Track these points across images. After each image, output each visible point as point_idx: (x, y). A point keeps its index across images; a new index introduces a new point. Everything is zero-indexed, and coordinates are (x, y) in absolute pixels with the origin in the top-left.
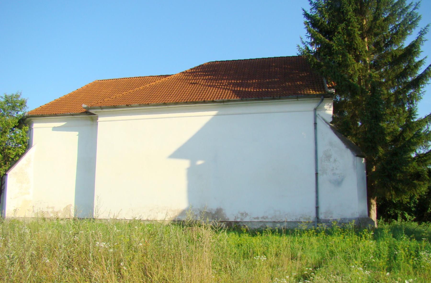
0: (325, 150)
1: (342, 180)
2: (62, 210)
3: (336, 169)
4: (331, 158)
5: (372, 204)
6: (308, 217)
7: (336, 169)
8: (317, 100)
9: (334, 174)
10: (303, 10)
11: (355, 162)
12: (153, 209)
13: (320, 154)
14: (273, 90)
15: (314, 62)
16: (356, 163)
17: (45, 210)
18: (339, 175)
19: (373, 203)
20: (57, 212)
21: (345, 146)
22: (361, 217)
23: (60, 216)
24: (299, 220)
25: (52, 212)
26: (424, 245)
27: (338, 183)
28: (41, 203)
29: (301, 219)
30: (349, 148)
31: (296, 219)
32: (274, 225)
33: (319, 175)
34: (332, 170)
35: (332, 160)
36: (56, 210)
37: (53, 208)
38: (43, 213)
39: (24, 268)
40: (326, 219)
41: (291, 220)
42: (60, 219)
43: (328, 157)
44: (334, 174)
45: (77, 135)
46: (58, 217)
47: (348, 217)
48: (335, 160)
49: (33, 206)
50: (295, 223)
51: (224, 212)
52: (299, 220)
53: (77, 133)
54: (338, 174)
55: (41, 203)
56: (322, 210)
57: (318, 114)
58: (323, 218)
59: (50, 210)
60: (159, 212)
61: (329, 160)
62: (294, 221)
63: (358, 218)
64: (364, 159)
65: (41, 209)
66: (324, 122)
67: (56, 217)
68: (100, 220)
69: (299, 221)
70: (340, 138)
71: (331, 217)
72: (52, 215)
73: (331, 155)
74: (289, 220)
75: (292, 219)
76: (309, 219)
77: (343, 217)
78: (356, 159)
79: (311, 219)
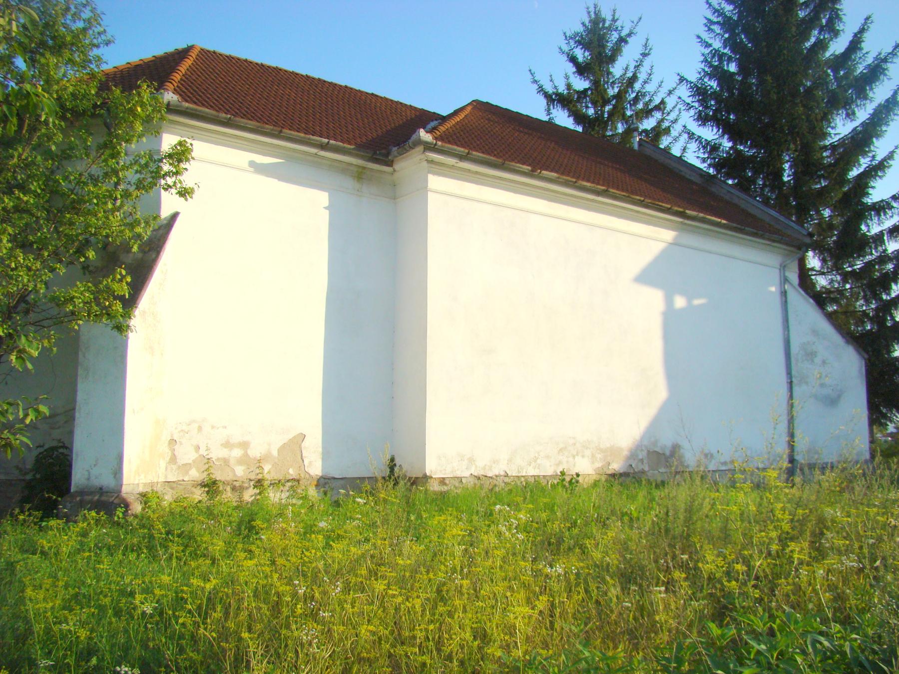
1: (839, 397)
2: (275, 453)
4: (816, 357)
10: (678, 74)
17: (217, 453)
20: (259, 461)
21: (844, 340)
23: (269, 471)
25: (240, 462)
27: (833, 401)
28: (200, 429)
30: (852, 344)
32: (812, 474)
35: (818, 360)
36: (255, 452)
37: (245, 445)
38: (207, 466)
42: (266, 483)
43: (811, 355)
44: (822, 385)
45: (325, 208)
49: (172, 442)
51: (682, 451)
53: (322, 198)
55: (200, 429)
56: (802, 443)
59: (237, 453)
60: (577, 454)
61: (813, 361)
65: (202, 451)
67: (253, 477)
68: (442, 481)
72: (240, 471)
73: (816, 352)
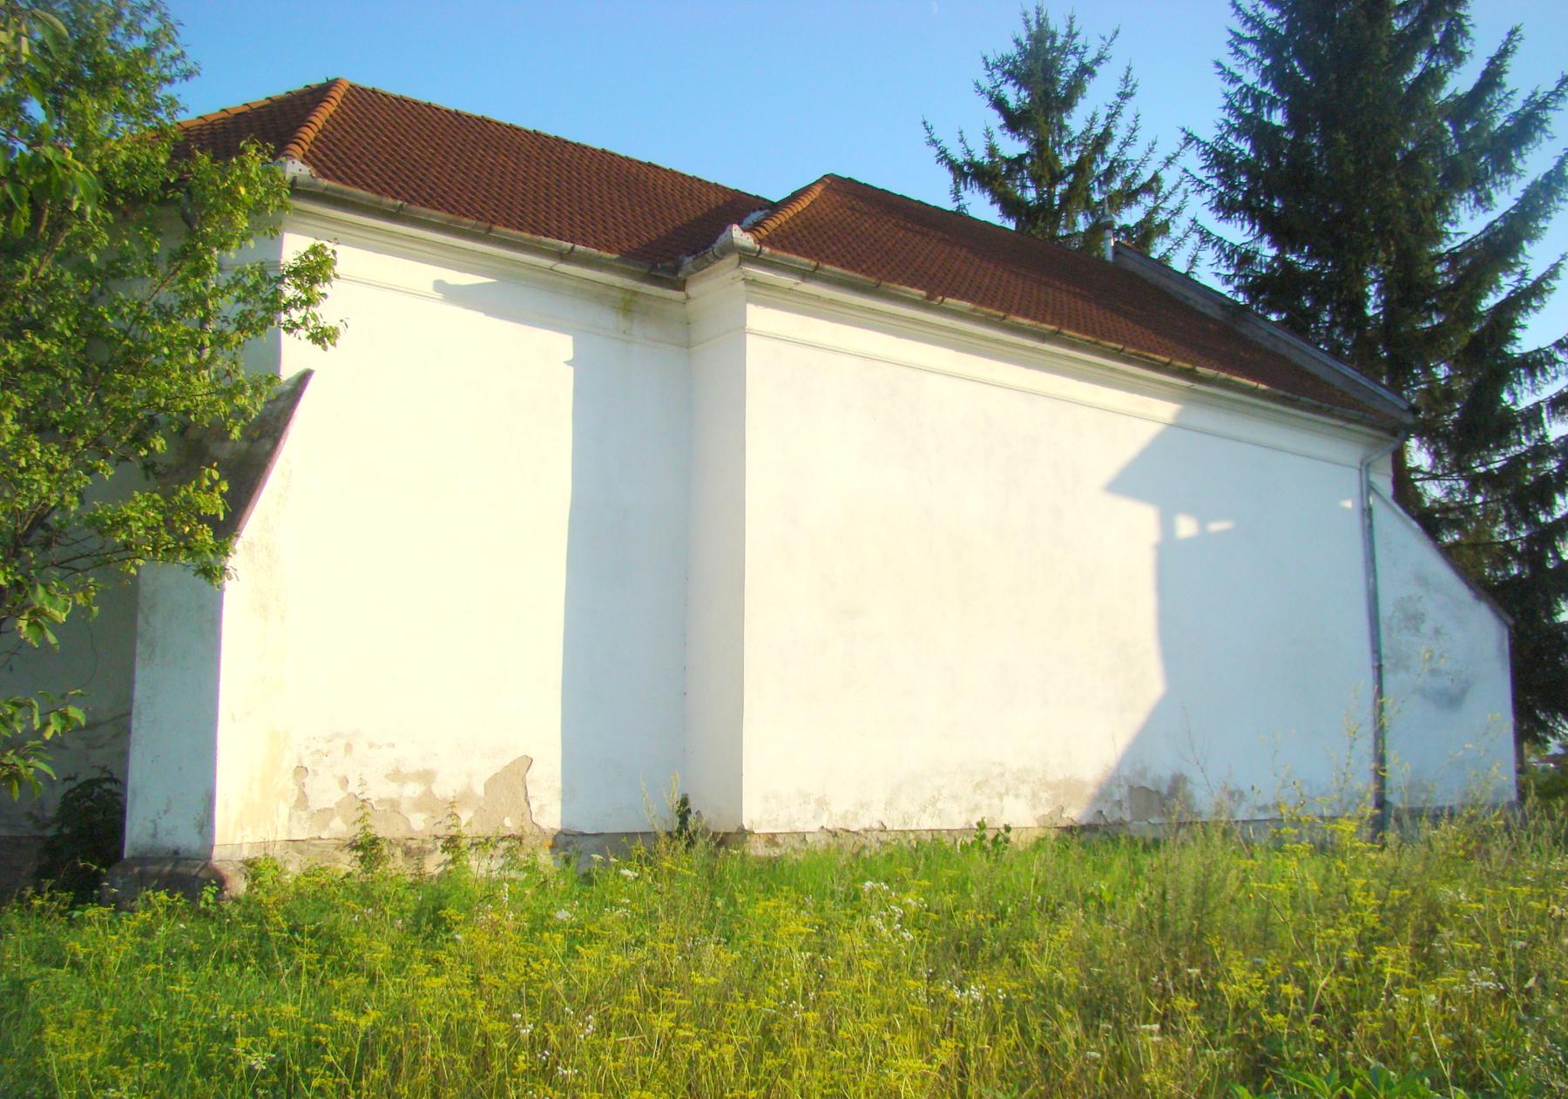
1: (1464, 692)
2: (479, 790)
8: (1369, 435)
9: (1434, 672)
12: (987, 781)
13: (1386, 608)
15: (87, 83)
20: (452, 804)
23: (469, 822)
25: (418, 805)
26: (1357, 833)
27: (1452, 700)
28: (349, 748)
35: (1426, 628)
36: (445, 788)
37: (426, 777)
38: (361, 813)
42: (464, 843)
43: (1414, 620)
44: (1434, 672)
45: (568, 363)
46: (453, 831)
49: (301, 771)
53: (561, 345)
54: (1448, 673)
56: (1398, 772)
59: (413, 790)
61: (1417, 630)
65: (353, 787)
72: (419, 822)
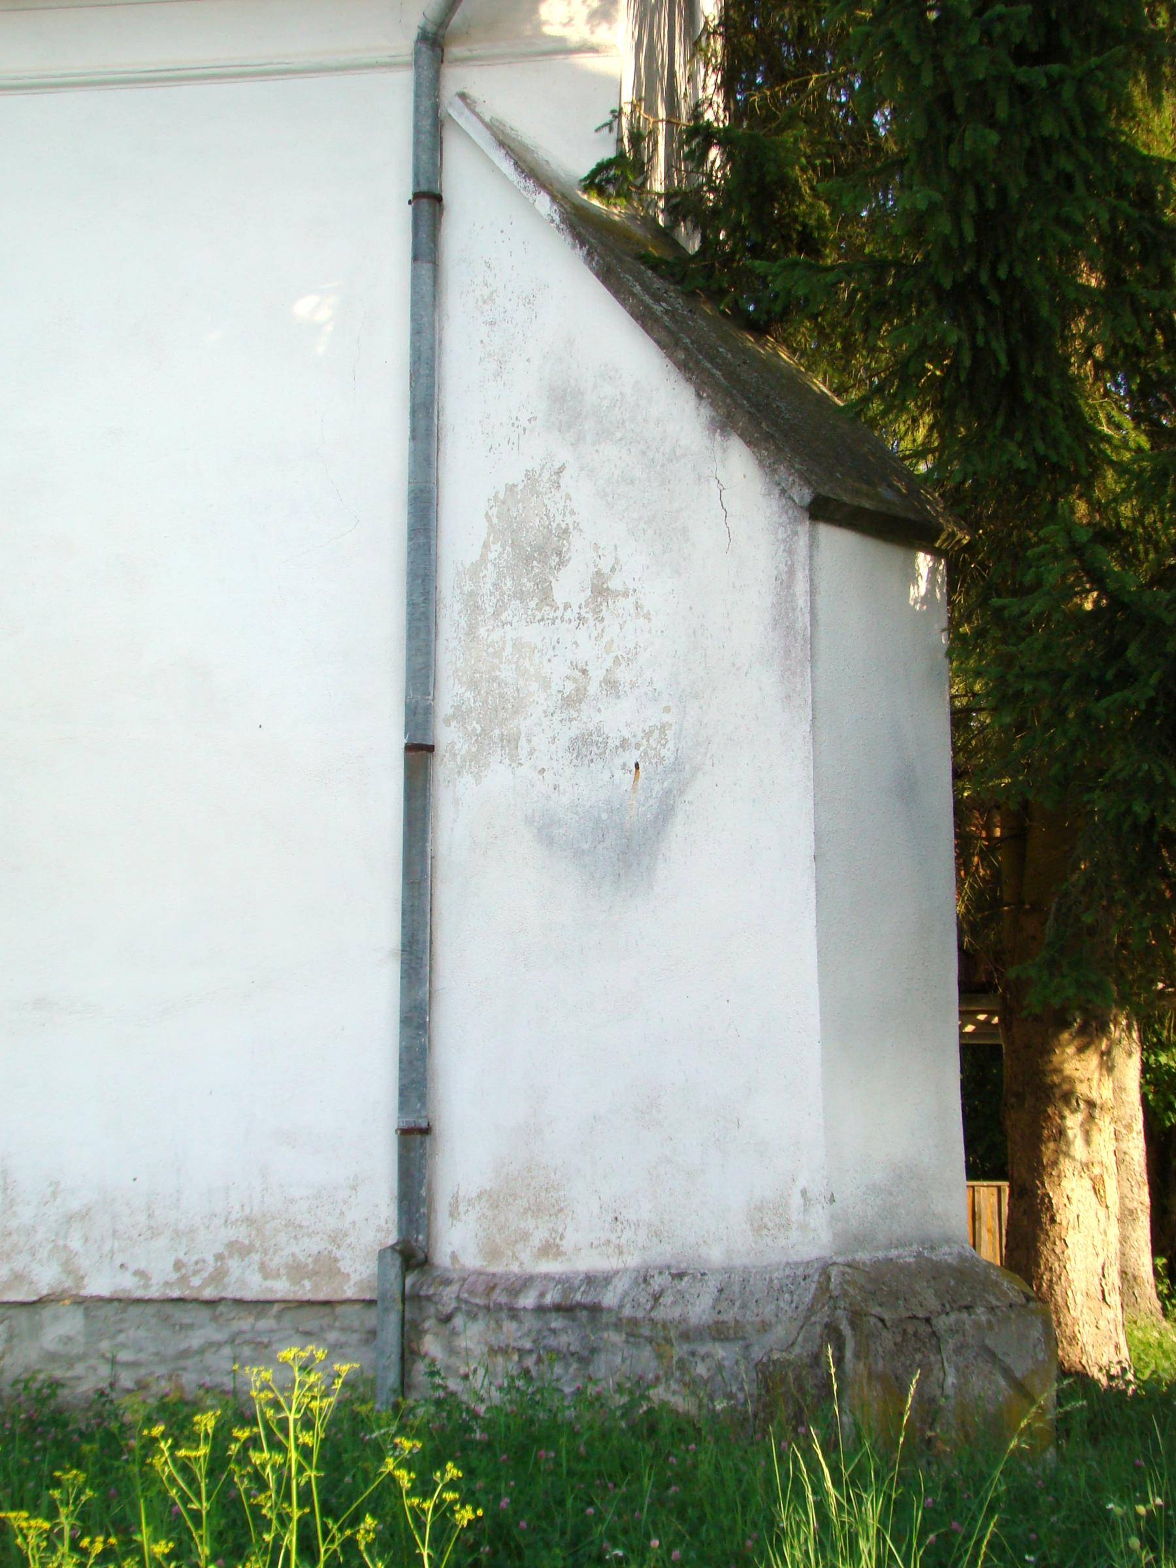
0: (511, 488)
1: (665, 813)
3: (611, 685)
5: (1068, 1097)
6: (314, 1245)
7: (611, 685)
11: (801, 587)
14: (1168, 891)
16: (813, 592)
18: (631, 757)
19: (1081, 1089)
21: (706, 412)
22: (863, 1256)
24: (218, 1276)
29: (234, 1264)
31: (178, 1265)
33: (443, 768)
34: (572, 702)
39: (547, 1241)
40: (497, 1268)
41: (128, 1284)
47: (715, 1255)
48: (600, 591)
50: (169, 1309)
52: (218, 1276)
54: (624, 744)
57: (463, 96)
58: (472, 1260)
61: (546, 596)
62: (154, 1292)
63: (825, 1269)
64: (923, 561)
66: (507, 167)
69: (208, 1293)
70: (644, 318)
71: (549, 1249)
74: (99, 1285)
75: (140, 1274)
76: (327, 1266)
77: (663, 1253)
78: (813, 544)
79: (345, 1266)
